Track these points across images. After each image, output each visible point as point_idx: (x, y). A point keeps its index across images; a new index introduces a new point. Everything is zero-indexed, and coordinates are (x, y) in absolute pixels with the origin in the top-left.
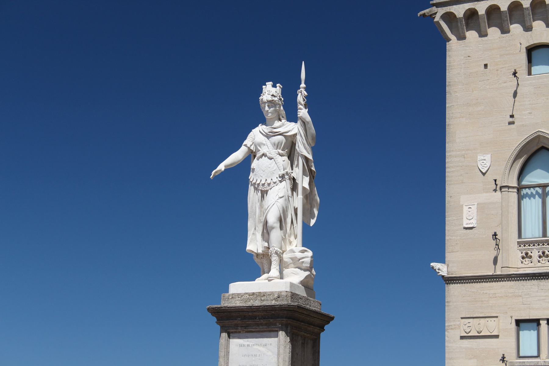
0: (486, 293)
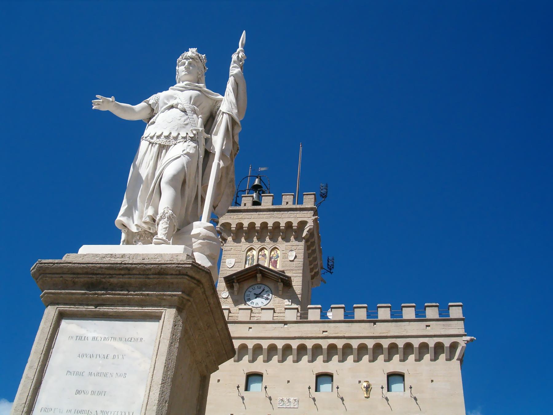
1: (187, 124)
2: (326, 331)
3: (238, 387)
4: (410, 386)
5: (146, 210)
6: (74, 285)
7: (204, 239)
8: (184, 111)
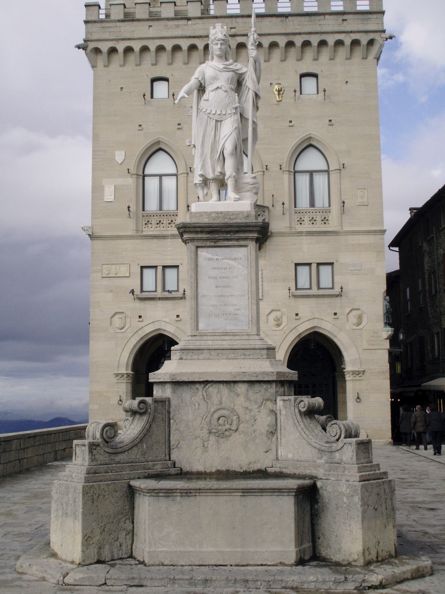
1: (229, 103)
3: (144, 95)
4: (323, 89)
6: (202, 232)
8: (226, 91)
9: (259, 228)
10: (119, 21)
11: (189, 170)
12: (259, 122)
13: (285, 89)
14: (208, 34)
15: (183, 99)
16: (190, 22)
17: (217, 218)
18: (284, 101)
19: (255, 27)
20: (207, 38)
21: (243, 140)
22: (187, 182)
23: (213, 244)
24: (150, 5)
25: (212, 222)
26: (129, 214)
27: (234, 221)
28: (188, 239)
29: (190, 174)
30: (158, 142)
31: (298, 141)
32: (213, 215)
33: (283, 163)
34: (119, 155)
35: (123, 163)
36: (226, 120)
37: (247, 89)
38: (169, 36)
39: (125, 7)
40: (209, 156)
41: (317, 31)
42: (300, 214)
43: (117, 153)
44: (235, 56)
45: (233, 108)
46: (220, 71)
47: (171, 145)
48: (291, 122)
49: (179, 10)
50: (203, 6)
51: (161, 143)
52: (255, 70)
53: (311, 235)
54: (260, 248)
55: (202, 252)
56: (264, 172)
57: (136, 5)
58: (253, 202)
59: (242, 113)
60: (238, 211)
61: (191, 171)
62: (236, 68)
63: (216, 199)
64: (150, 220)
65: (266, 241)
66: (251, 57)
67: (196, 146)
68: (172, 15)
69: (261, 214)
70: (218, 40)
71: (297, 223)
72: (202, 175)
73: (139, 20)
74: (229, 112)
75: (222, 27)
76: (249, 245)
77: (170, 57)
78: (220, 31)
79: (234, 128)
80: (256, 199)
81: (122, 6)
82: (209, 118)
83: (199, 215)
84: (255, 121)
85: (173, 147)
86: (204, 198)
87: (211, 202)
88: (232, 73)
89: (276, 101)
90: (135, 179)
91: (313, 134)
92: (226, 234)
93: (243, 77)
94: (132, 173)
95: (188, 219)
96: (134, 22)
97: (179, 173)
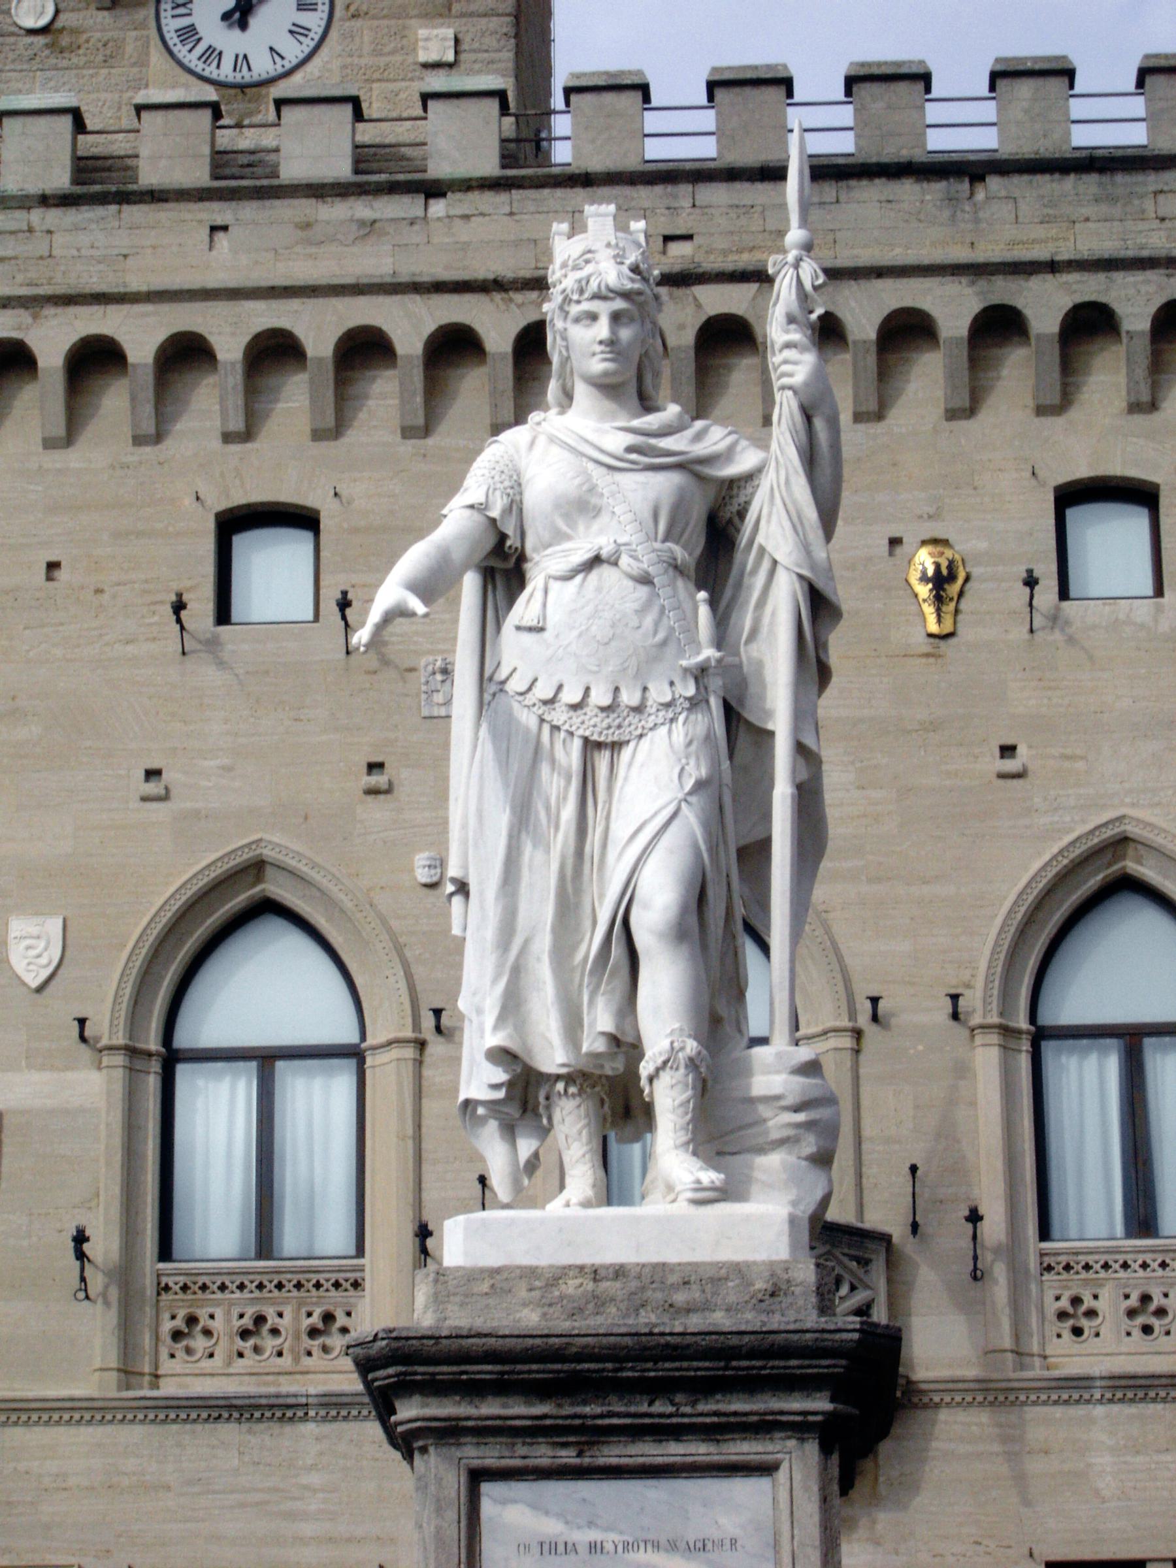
0: (27, 1473)
1: (664, 643)
2: (689, 237)
3: (179, 607)
5: (589, 1013)
6: (501, 1388)
7: (796, 1109)
8: (645, 580)
9: (843, 1362)
10: (45, 200)
11: (428, 1021)
12: (829, 754)
13: (976, 571)
14: (541, 273)
15: (400, 625)
16: (438, 208)
17: (591, 1306)
18: (966, 633)
19: (804, 222)
20: (534, 295)
21: (742, 853)
22: (418, 1095)
23: (568, 1457)
24: (217, 114)
25: (565, 1326)
26: (83, 1279)
27: (695, 1322)
28: (419, 1429)
29: (437, 1048)
30: (257, 868)
31: (1054, 857)
32: (570, 1287)
33: (968, 986)
34: (28, 942)
35: (53, 983)
36: (645, 743)
37: (766, 565)
38: (324, 281)
39: (79, 125)
40: (543, 943)
41: (1145, 253)
42: (1071, 1275)
43: (18, 926)
44: (689, 389)
45: (686, 670)
46: (611, 468)
47: (324, 882)
48: (1008, 751)
49: (378, 140)
50: (512, 119)
51: (269, 872)
52: (810, 458)
53: (1141, 1394)
54: (847, 1484)
55: (504, 1502)
56: (858, 1034)
57: (144, 115)
58: (808, 1207)
59: (733, 703)
60: (719, 1265)
61: (438, 1029)
62: (701, 449)
63: (590, 1193)
64: (202, 1314)
65: (883, 1432)
66: (783, 388)
67: (473, 889)
68: (341, 169)
69: (847, 1276)
70: (597, 296)
71: (1053, 1326)
72: (503, 1056)
73: (155, 196)
74: (659, 693)
75: (621, 226)
76: (785, 1467)
77: (330, 394)
78: (608, 245)
79: (689, 784)
80: (819, 1194)
81: (67, 122)
82: (546, 729)
83: (485, 1287)
84: (809, 741)
85: (342, 896)
86: (517, 1187)
87: (555, 1207)
88: (674, 479)
89: (921, 638)
90: (119, 1074)
91: (1138, 820)
92: (646, 1399)
93: (742, 499)
94: (104, 1042)
95: (426, 1307)
96: (126, 208)
97: (370, 1041)
